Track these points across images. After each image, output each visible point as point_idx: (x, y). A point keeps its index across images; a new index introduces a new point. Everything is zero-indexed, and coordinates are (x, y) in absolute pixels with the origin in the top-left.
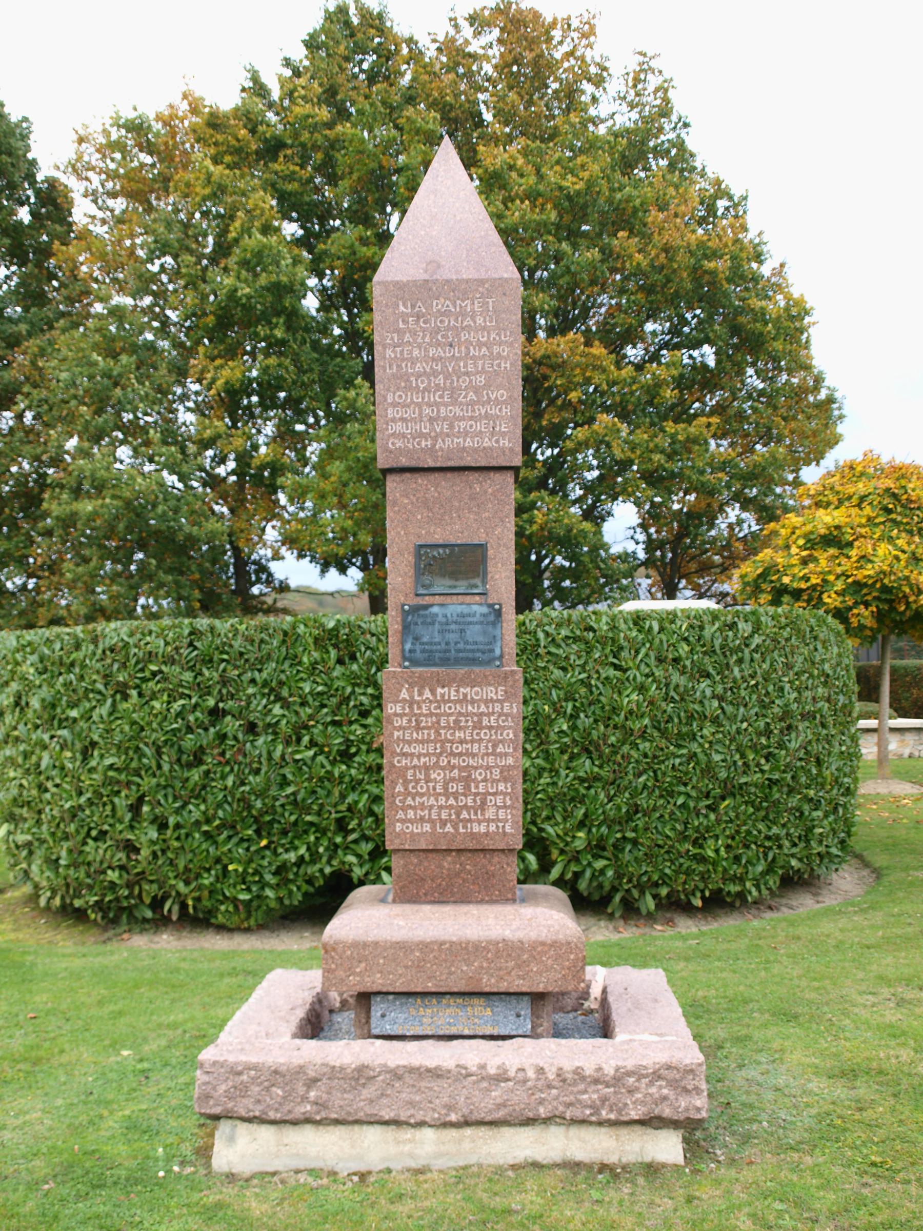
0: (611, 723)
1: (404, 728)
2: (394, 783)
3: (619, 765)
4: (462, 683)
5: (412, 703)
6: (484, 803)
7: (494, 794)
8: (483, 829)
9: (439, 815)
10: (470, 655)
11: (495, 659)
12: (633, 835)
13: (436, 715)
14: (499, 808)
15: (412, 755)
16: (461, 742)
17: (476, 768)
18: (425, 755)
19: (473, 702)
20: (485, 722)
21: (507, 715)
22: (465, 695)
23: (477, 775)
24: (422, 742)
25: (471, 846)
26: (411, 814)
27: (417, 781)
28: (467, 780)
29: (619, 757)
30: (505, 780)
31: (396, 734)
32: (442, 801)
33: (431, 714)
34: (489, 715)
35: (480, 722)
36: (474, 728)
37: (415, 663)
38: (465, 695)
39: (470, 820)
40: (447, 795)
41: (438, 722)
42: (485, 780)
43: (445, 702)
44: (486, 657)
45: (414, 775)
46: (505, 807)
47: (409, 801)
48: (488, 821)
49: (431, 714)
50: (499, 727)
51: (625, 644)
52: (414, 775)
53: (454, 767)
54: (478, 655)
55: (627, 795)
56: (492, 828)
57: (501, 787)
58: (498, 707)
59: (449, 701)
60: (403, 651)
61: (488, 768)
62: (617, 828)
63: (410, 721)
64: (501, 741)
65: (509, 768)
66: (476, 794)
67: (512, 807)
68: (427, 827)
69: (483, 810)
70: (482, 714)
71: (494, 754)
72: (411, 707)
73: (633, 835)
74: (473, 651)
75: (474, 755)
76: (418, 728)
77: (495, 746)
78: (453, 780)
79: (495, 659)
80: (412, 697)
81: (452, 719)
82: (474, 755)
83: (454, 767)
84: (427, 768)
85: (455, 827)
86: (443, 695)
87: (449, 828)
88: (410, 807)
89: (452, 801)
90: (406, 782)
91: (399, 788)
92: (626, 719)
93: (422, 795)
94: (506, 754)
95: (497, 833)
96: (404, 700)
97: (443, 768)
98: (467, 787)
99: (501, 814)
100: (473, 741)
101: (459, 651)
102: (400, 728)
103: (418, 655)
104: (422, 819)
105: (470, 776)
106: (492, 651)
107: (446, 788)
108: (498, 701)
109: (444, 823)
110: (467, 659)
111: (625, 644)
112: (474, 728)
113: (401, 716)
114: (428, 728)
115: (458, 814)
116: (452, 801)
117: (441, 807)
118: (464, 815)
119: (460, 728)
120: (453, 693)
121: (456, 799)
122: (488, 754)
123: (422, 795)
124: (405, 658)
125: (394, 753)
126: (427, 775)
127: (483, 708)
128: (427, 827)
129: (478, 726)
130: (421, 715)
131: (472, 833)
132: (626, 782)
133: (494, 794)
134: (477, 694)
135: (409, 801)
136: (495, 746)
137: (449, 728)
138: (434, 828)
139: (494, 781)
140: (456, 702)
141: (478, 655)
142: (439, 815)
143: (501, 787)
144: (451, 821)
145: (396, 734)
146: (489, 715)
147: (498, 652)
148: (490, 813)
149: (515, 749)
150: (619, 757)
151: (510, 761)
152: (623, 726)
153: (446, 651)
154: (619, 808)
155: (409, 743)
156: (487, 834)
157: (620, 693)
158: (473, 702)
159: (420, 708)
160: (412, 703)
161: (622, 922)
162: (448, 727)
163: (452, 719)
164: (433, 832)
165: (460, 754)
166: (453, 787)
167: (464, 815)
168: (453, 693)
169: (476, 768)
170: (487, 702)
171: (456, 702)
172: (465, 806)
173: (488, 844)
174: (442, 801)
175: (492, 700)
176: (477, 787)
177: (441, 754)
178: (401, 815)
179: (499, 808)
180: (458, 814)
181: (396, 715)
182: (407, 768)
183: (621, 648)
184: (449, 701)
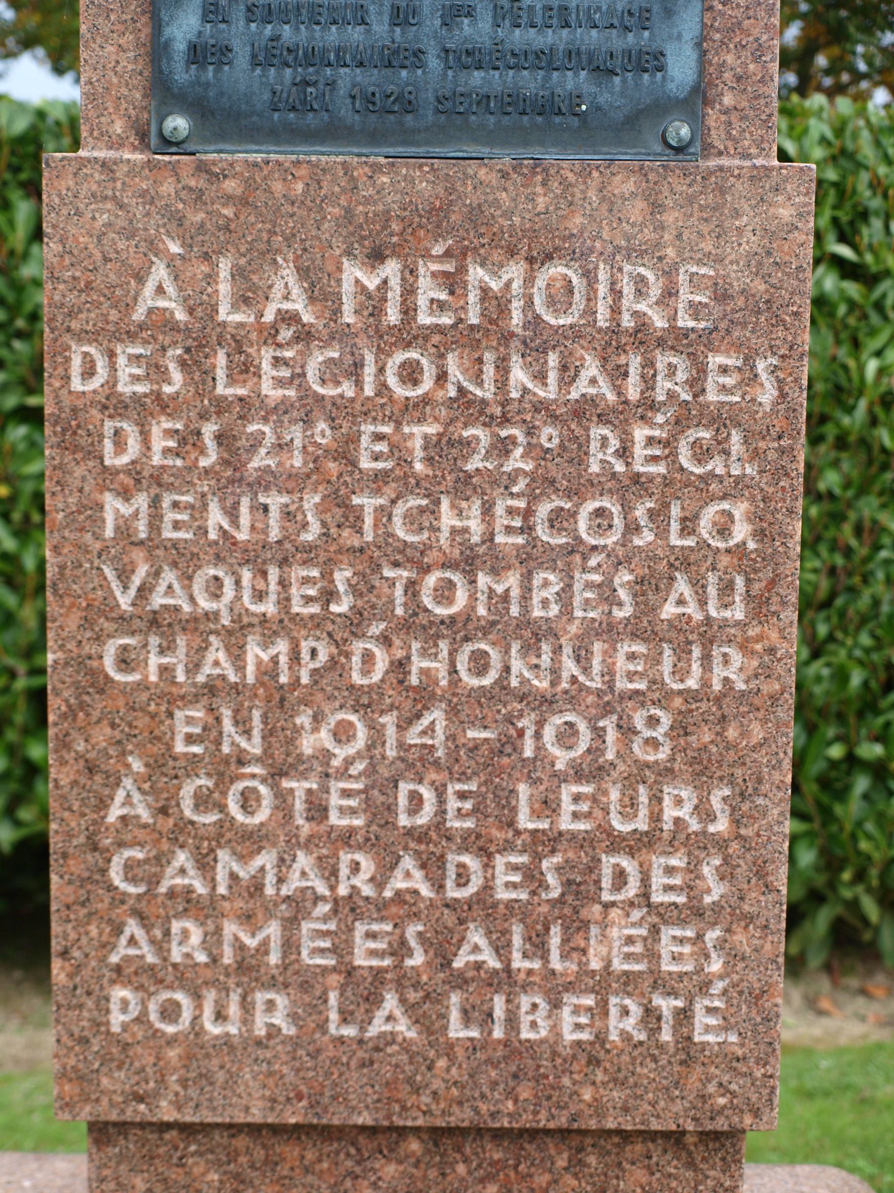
0: (830, 430)
1: (158, 480)
2: (99, 774)
3: (848, 552)
4: (481, 237)
5: (199, 341)
6: (580, 889)
7: (640, 844)
8: (572, 1027)
9: (341, 948)
10: (529, 82)
11: (663, 107)
12: (878, 750)
13: (337, 412)
14: (663, 915)
15: (199, 625)
16: (468, 562)
17: (546, 704)
18: (270, 631)
19: (537, 342)
20: (601, 451)
21: (720, 420)
22: (496, 304)
23: (552, 742)
24: (255, 557)
25: (507, 1113)
26: (188, 940)
27: (226, 769)
28: (495, 766)
29: (847, 529)
30: (702, 770)
31: (113, 507)
32: (359, 873)
33: (309, 408)
34: (619, 416)
35: (575, 451)
36: (542, 484)
37: (222, 120)
38: (496, 304)
39: (505, 980)
40: (382, 840)
41: (345, 451)
42: (591, 770)
43: (388, 340)
44: (613, 95)
45: (211, 733)
46: (695, 912)
47: (181, 871)
48: (603, 984)
49: (309, 408)
50: (675, 483)
51: (876, 203)
52: (211, 733)
53: (424, 697)
54: (574, 81)
55: (865, 639)
56: (624, 1022)
57: (679, 805)
58: (672, 378)
59: (408, 334)
60: (157, 50)
61: (611, 701)
62: (831, 732)
63: (188, 441)
64: (684, 561)
65: (723, 705)
66: (545, 842)
67: (731, 914)
68: (275, 1012)
69: (576, 926)
70: (585, 411)
71: (644, 628)
72: (195, 364)
73: (878, 750)
74: (543, 60)
75: (533, 633)
76: (232, 477)
77: (650, 587)
78: (418, 762)
79: (663, 107)
80: (202, 308)
81: (418, 433)
82: (533, 633)
83: (424, 697)
84: (279, 699)
85: (426, 1012)
86: (373, 303)
87: (391, 1018)
88: (187, 902)
89: (408, 877)
90: (164, 771)
91: (128, 802)
92: (874, 421)
93: (251, 841)
94: (709, 634)
95: (650, 1050)
96: (160, 322)
97: (365, 702)
98: (495, 806)
99: (674, 949)
100: (530, 559)
101: (470, 58)
102: (136, 478)
103: (240, 76)
104: (248, 967)
105: (509, 743)
106: (651, 61)
107: (381, 813)
108: (675, 340)
109: (364, 993)
110: (514, 103)
111: (876, 203)
112: (542, 484)
113: (143, 410)
114: (295, 483)
115: (442, 949)
116: (408, 877)
117: (350, 908)
118: (476, 949)
119: (464, 486)
120: (428, 290)
121: (432, 866)
122: (609, 631)
123: (251, 841)
124: (163, 92)
125: (99, 615)
126: (282, 737)
127: (591, 380)
128: (275, 1012)
129: (558, 472)
130: (246, 407)
131: (514, 1048)
132: (864, 602)
133: (640, 844)
134: (561, 296)
135: (181, 871)
136: (650, 587)
137: (409, 484)
138: (309, 1013)
139: (639, 774)
140: (441, 340)
141: (574, 81)
142: (341, 948)
143: (679, 805)
144: (404, 981)
145: (113, 507)
146: (619, 416)
147: (681, 69)
148: (613, 944)
149: (759, 606)
150: (847, 529)
151: (732, 668)
152: (864, 443)
153: (391, 58)
154: (841, 676)
155: (185, 560)
156: (593, 1053)
157: (856, 344)
158: (537, 342)
159: (244, 369)
160: (199, 341)
161: (824, 983)
162: (397, 479)
163: (418, 433)
164: (308, 1040)
165: (461, 628)
166: (418, 805)
167: (476, 949)
168: (428, 290)
169: (546, 704)
170: (613, 344)
171: (441, 340)
172: (483, 904)
173: (594, 1100)
174: (359, 873)
175: (641, 334)
176: (547, 806)
177: (355, 623)
178: (134, 943)
179: (663, 915)
180: (442, 949)
181: (113, 404)
182: (171, 698)
183: (864, 215)
184: (408, 334)
